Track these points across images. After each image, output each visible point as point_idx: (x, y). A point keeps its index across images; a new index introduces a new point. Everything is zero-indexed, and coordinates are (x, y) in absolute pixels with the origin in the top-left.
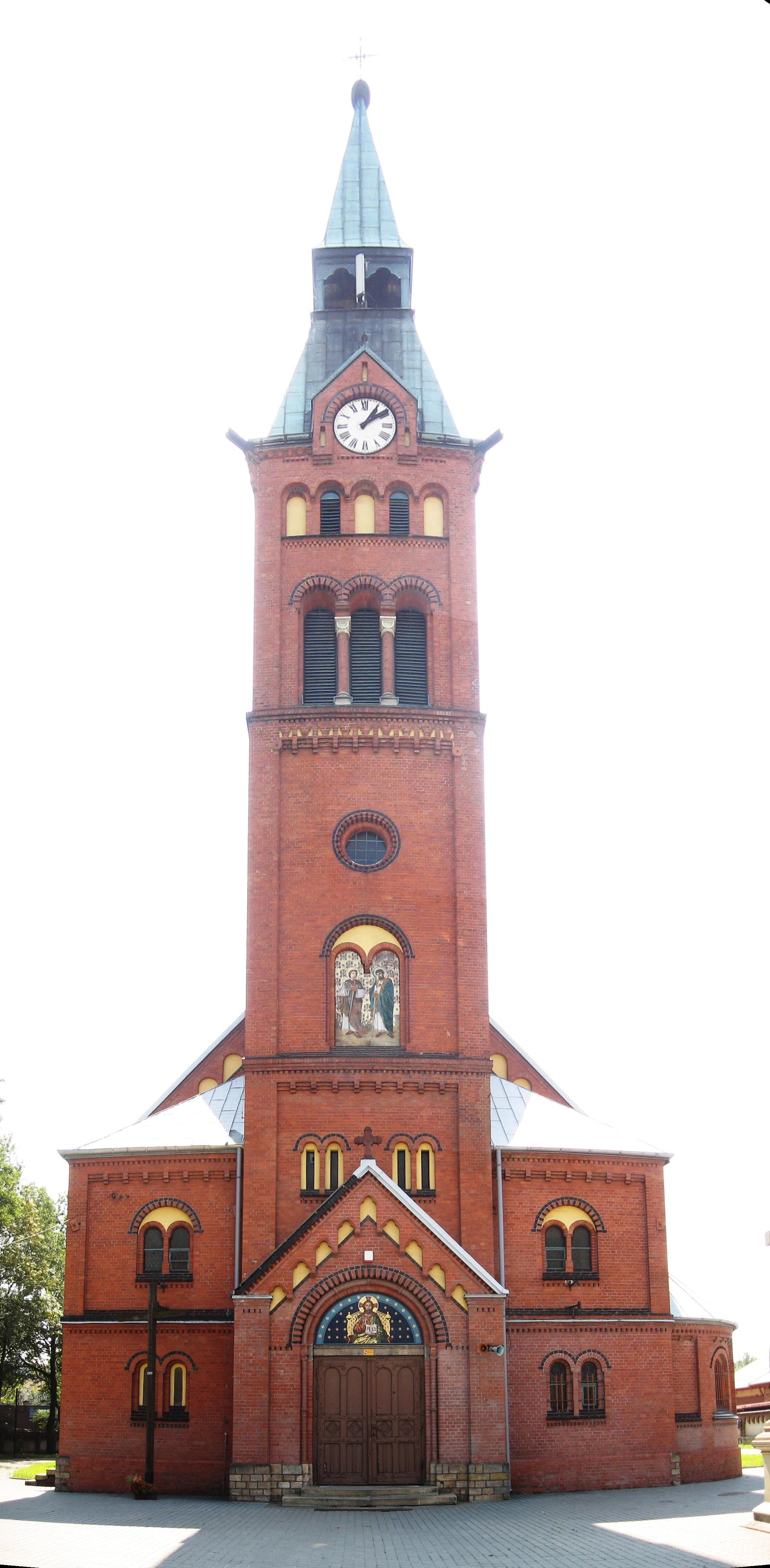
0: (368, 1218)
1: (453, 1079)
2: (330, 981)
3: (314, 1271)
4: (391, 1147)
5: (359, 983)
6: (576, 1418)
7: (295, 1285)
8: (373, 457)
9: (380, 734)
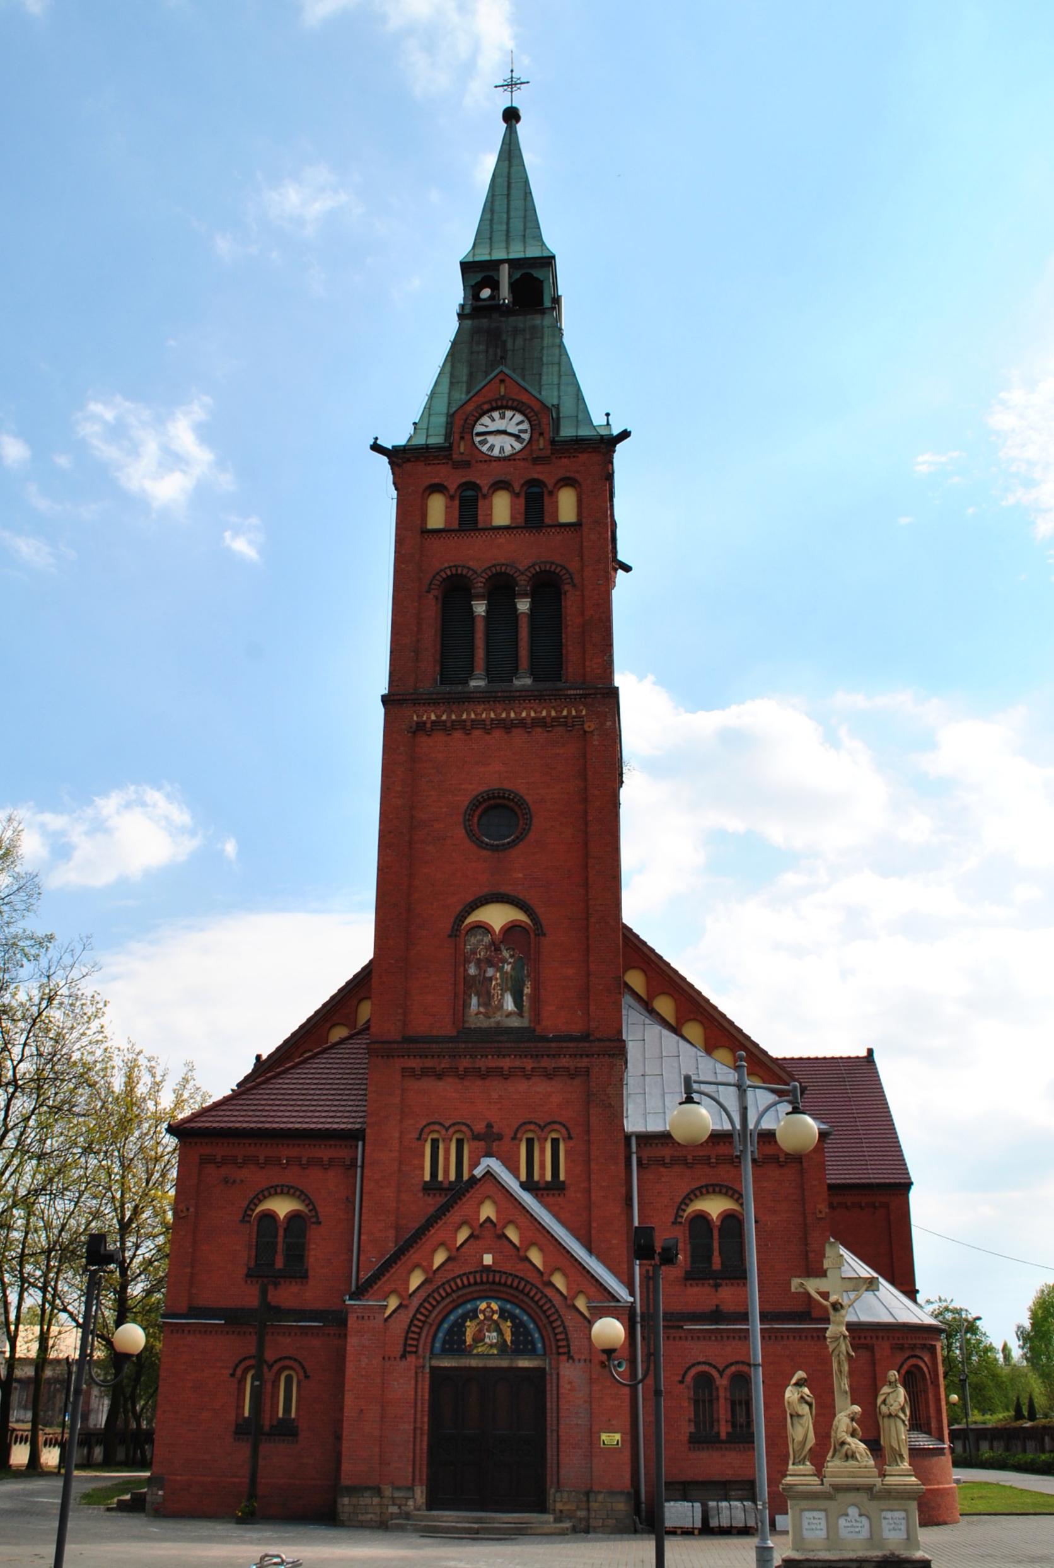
0: (488, 1219)
3: (431, 1275)
9: (513, 715)
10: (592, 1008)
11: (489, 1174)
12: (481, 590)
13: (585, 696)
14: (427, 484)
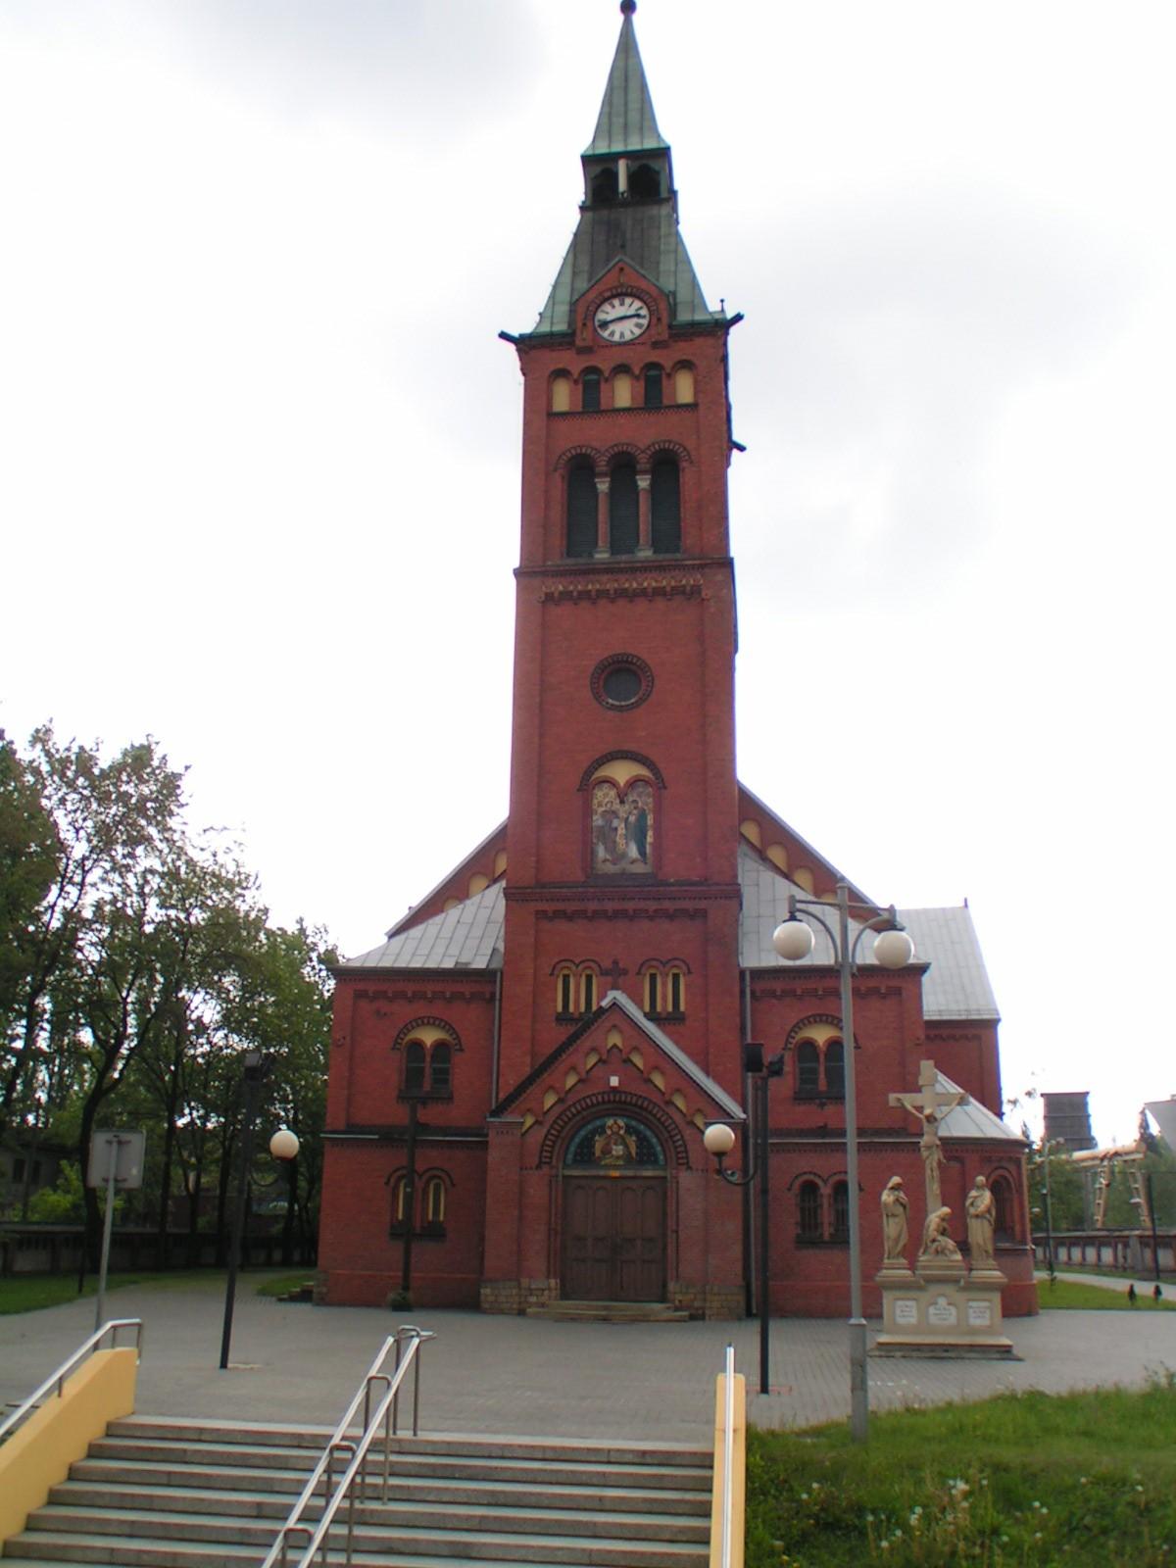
0: (615, 1046)
1: (702, 904)
2: (587, 811)
4: (643, 971)
5: (615, 813)
6: (823, 1242)
7: (545, 1109)
11: (614, 1005)
12: (604, 469)
14: (552, 368)
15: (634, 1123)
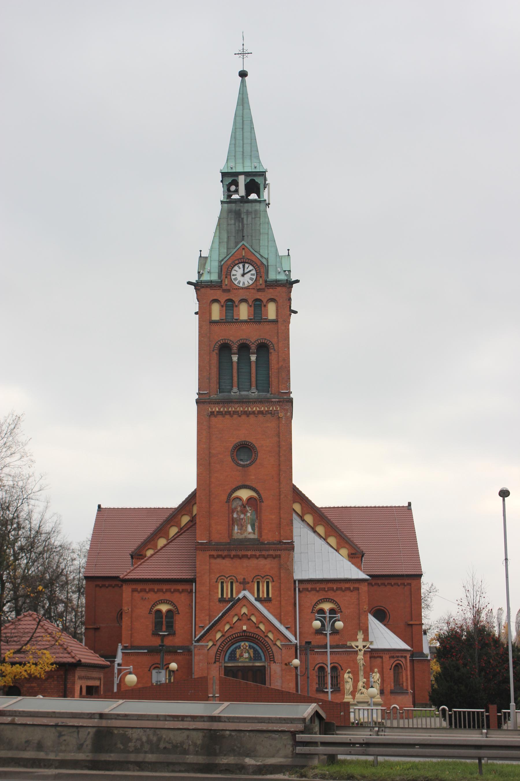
0: (244, 613)
1: (279, 553)
8: (247, 288)
9: (250, 409)
10: (282, 532)
11: (245, 597)
12: (236, 351)
13: (279, 402)
14: (212, 299)
15: (252, 644)
